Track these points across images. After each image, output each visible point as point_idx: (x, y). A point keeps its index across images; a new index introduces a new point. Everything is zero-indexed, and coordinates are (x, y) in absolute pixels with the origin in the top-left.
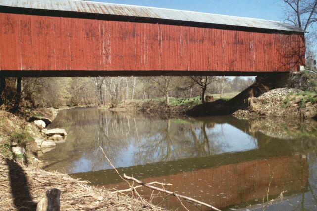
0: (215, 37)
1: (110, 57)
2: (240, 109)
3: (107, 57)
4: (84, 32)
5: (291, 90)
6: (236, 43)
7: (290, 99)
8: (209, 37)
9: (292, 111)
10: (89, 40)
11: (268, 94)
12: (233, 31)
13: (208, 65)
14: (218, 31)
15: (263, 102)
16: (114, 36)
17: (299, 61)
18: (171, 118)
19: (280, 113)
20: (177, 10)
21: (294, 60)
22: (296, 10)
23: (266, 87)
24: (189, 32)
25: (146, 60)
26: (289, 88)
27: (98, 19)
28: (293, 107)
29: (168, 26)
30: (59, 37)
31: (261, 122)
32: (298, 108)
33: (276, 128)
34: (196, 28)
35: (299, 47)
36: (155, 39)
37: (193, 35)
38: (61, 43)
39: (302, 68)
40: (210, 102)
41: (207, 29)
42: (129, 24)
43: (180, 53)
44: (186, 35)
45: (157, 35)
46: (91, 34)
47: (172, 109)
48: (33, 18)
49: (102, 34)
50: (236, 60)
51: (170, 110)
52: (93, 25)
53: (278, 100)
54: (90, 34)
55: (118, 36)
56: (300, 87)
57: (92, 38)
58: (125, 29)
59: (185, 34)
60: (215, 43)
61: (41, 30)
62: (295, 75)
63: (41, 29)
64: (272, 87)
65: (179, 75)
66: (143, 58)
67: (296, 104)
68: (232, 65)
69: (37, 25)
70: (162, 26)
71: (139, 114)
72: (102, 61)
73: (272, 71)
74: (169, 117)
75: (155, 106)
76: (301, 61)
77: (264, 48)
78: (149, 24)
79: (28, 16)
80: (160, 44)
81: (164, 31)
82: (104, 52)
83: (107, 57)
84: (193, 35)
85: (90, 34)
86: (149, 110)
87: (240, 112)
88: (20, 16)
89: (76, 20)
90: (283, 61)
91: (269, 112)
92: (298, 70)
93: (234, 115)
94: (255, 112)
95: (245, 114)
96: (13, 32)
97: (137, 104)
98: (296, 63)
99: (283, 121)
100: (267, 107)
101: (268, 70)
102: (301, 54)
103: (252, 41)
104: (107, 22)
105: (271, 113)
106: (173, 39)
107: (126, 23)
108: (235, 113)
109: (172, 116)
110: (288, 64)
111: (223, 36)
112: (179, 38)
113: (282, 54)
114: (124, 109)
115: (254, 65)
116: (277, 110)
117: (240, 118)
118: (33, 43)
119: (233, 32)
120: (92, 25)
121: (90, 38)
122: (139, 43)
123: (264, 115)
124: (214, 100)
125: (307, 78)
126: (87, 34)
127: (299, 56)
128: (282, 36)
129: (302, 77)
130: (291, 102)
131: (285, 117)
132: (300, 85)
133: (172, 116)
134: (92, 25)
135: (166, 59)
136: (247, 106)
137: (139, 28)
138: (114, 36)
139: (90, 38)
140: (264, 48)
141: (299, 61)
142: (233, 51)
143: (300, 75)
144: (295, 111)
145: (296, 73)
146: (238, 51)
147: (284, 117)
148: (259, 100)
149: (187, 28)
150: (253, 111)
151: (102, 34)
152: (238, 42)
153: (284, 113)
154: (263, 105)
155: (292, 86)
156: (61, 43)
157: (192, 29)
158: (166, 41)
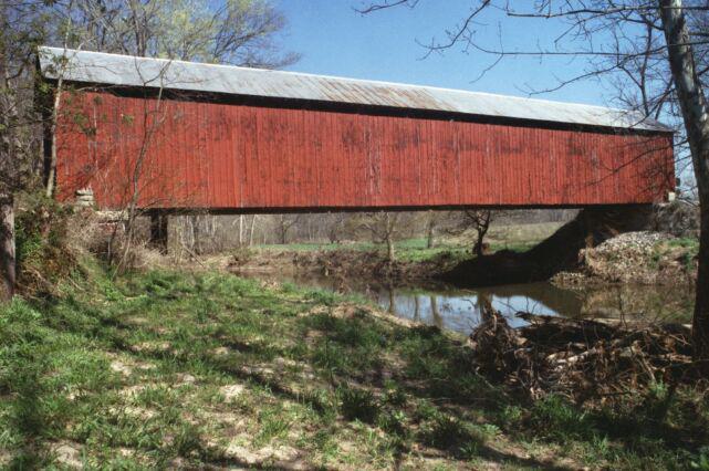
4: (340, 137)
5: (656, 236)
9: (672, 275)
10: (348, 151)
11: (618, 242)
15: (609, 257)
16: (387, 143)
18: (400, 287)
23: (613, 231)
25: (437, 187)
27: (361, 114)
28: (672, 267)
29: (468, 124)
33: (637, 304)
34: (510, 128)
36: (449, 149)
39: (672, 196)
40: (487, 256)
41: (528, 130)
42: (408, 121)
44: (497, 139)
46: (350, 139)
47: (404, 269)
51: (399, 272)
53: (639, 254)
54: (349, 140)
55: (391, 143)
56: (670, 229)
62: (663, 208)
64: (625, 228)
66: (431, 181)
68: (565, 194)
70: (460, 124)
71: (310, 278)
72: (369, 189)
73: (626, 202)
74: (395, 285)
75: (354, 263)
77: (613, 162)
79: (253, 109)
82: (371, 173)
83: (376, 182)
85: (349, 140)
86: (340, 269)
87: (566, 275)
88: (241, 108)
91: (628, 276)
95: (579, 281)
96: (230, 138)
97: (304, 258)
98: (662, 186)
100: (620, 266)
102: (669, 169)
104: (376, 118)
106: (477, 148)
108: (557, 278)
113: (640, 171)
119: (566, 134)
121: (350, 147)
122: (425, 156)
123: (618, 280)
124: (493, 252)
125: (683, 215)
126: (345, 141)
127: (665, 172)
130: (666, 258)
131: (660, 285)
132: (671, 225)
133: (404, 281)
136: (577, 264)
139: (350, 147)
143: (672, 209)
145: (663, 205)
147: (659, 285)
148: (600, 254)
149: (497, 127)
150: (595, 275)
152: (574, 151)
155: (657, 229)
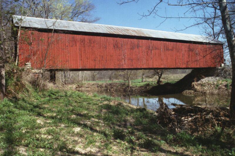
0: (178, 47)
1: (126, 60)
2: (186, 89)
3: (125, 60)
5: (218, 78)
6: (189, 51)
7: (219, 84)
8: (176, 48)
9: (223, 91)
11: (205, 80)
12: (188, 44)
13: (175, 64)
14: (181, 43)
15: (202, 85)
16: (128, 47)
17: (221, 61)
18: (133, 95)
19: (216, 92)
20: (149, 30)
21: (218, 60)
22: (212, 28)
23: (203, 76)
24: (166, 45)
26: (216, 77)
27: (120, 38)
30: (99, 48)
31: (202, 97)
32: (226, 89)
33: (211, 101)
35: (221, 53)
37: (168, 46)
38: (101, 52)
39: (223, 65)
41: (175, 43)
42: (135, 40)
43: (161, 58)
45: (150, 47)
47: (134, 89)
48: (87, 37)
49: (122, 46)
50: (189, 61)
52: (118, 41)
53: (212, 84)
54: (116, 47)
55: (130, 47)
56: (222, 76)
57: (117, 49)
58: (133, 43)
59: (164, 46)
60: (179, 51)
61: (90, 45)
62: (220, 69)
63: (90, 44)
65: (148, 69)
67: (224, 87)
69: (88, 41)
72: (122, 62)
73: (207, 67)
74: (131, 95)
76: (222, 60)
77: (203, 53)
78: (146, 40)
80: (151, 52)
81: (153, 45)
83: (125, 60)
84: (168, 46)
85: (116, 47)
87: (188, 91)
89: (109, 38)
90: (213, 60)
91: (208, 91)
92: (221, 66)
93: (184, 93)
94: (199, 92)
95: (192, 93)
96: (76, 46)
97: (101, 85)
99: (217, 97)
100: (206, 88)
101: (205, 67)
103: (197, 49)
105: (209, 92)
106: (158, 49)
107: (134, 39)
108: (185, 92)
109: (134, 93)
110: (215, 63)
111: (183, 47)
112: (161, 48)
114: (89, 89)
115: (198, 64)
116: (213, 90)
117: (188, 95)
118: (86, 52)
120: (116, 41)
121: (116, 49)
123: (205, 93)
125: (227, 71)
126: (114, 47)
127: (221, 58)
128: (211, 46)
129: (224, 70)
130: (221, 85)
131: (219, 94)
132: (223, 75)
133: (134, 93)
134: (116, 41)
135: (154, 61)
136: (191, 88)
137: (141, 43)
138: (128, 47)
139: (116, 49)
140: (203, 53)
141: (221, 61)
142: (188, 55)
143: (223, 69)
144: (225, 91)
145: (220, 68)
146: (190, 55)
147: (218, 94)
149: (165, 42)
150: (197, 91)
151: (122, 46)
152: (190, 50)
153: (218, 92)
154: (202, 87)
155: (218, 76)
156: (101, 52)
157: (167, 43)
158: (154, 50)
